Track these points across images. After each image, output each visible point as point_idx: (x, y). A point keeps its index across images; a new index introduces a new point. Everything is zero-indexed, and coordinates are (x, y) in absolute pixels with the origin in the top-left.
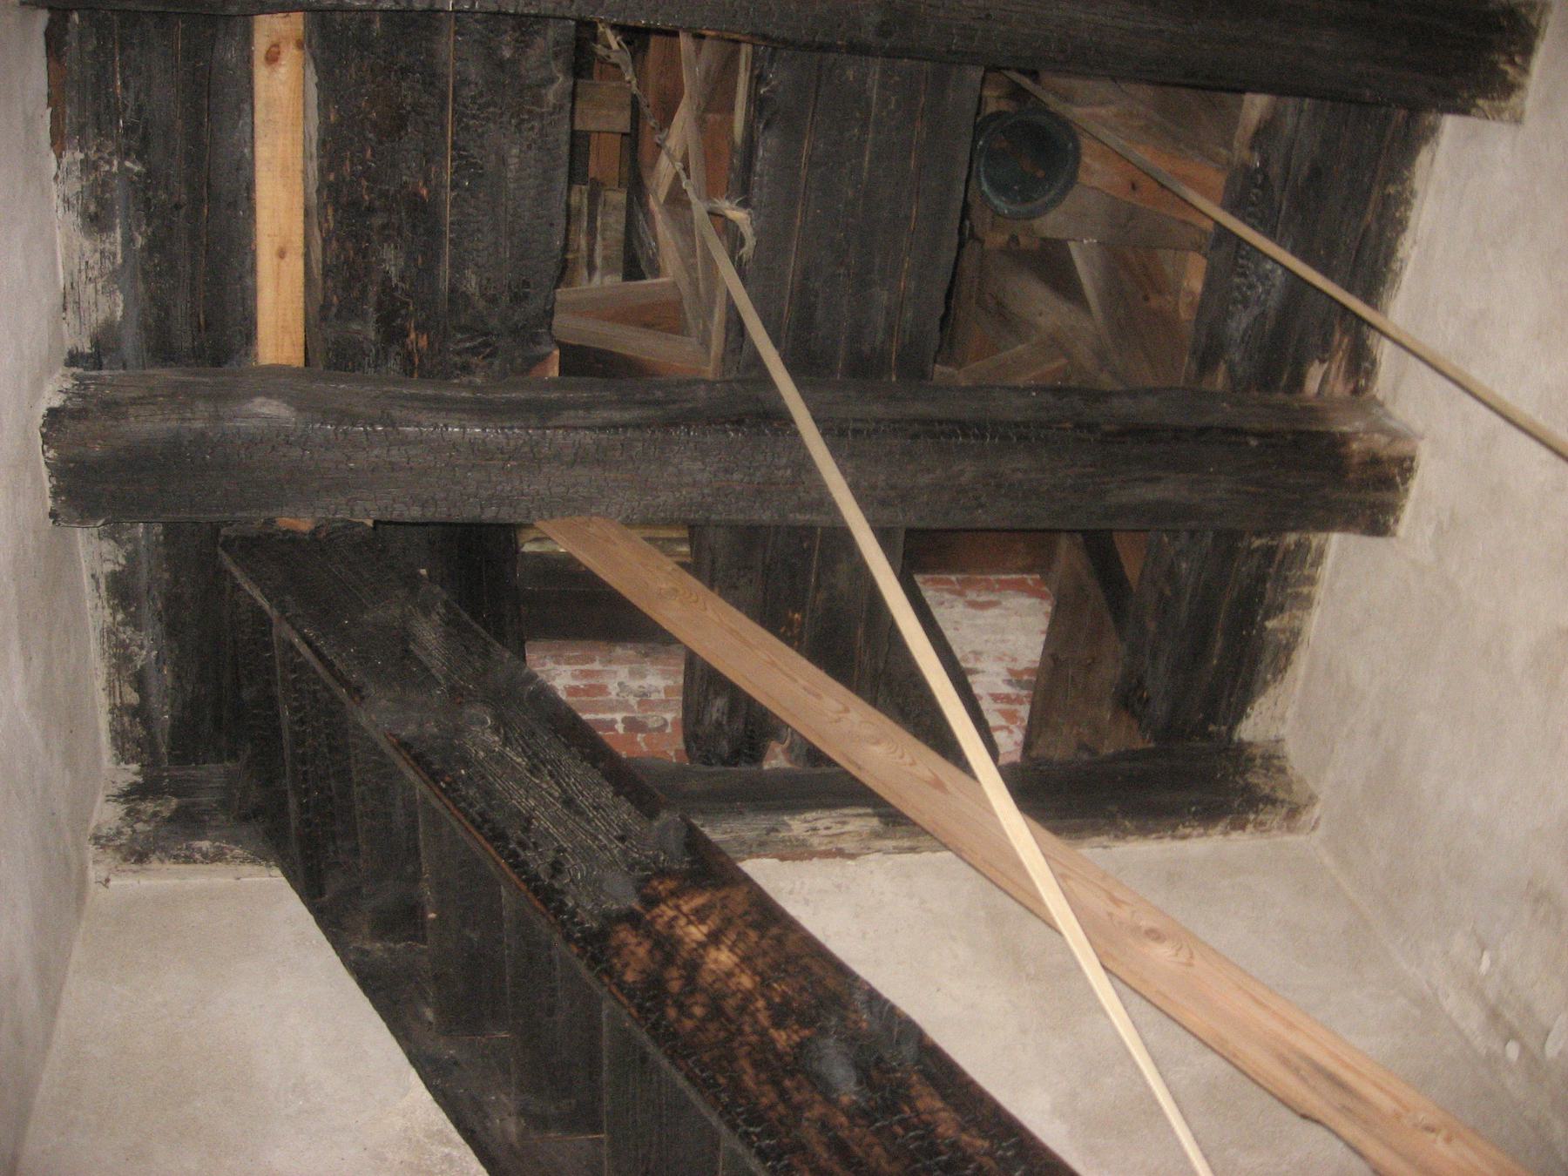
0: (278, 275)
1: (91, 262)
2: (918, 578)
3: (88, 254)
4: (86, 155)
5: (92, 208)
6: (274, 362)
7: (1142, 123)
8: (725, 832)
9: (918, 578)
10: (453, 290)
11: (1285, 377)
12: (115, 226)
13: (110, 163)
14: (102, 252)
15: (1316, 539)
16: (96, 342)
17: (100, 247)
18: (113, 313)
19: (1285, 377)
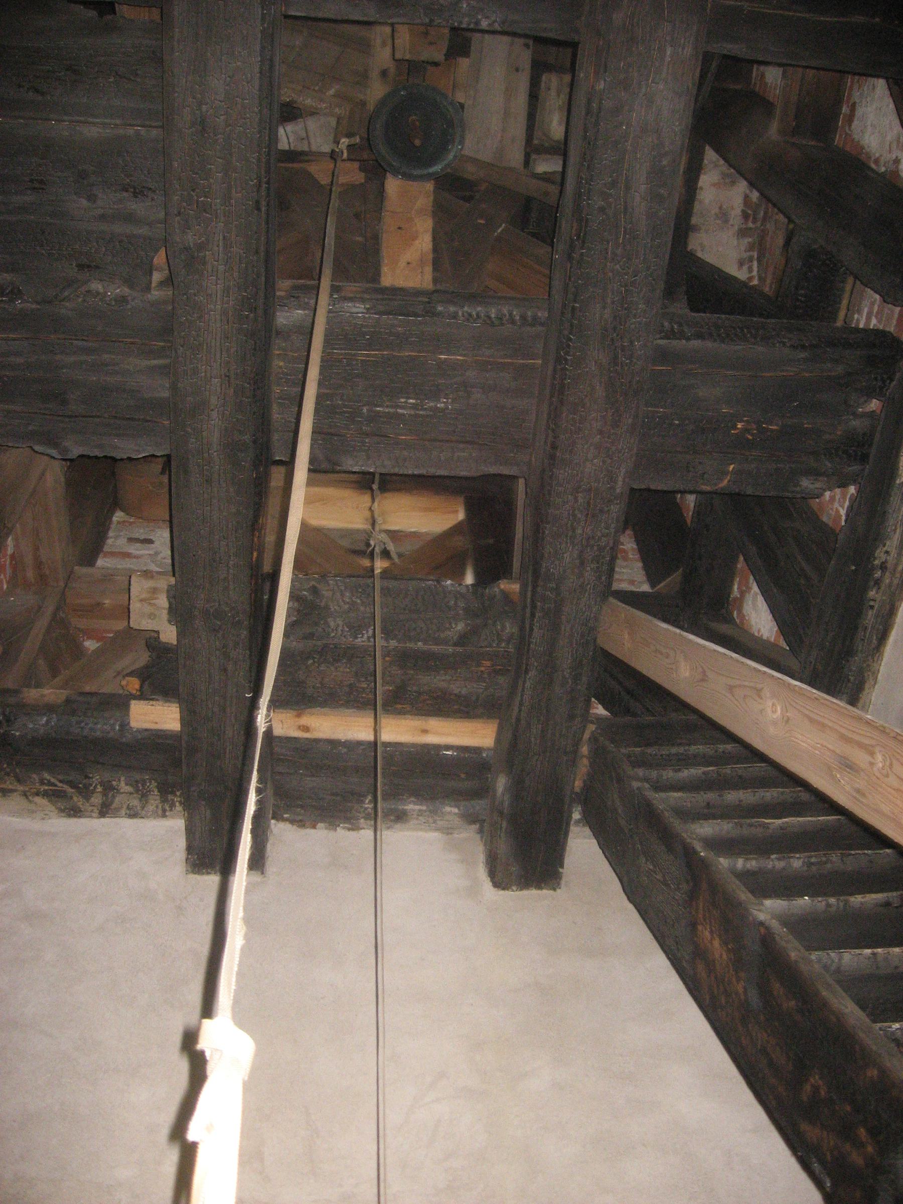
0: (436, 733)
1: (424, 821)
2: (710, 155)
3: (420, 822)
4: (362, 818)
5: (392, 818)
6: (494, 740)
7: (712, 166)
8: (895, 530)
9: (710, 155)
10: (455, 644)
11: (378, 409)
12: (403, 809)
13: (366, 809)
14: (418, 815)
15: (179, 808)
16: (474, 822)
17: (415, 816)
18: (455, 814)
19: (378, 409)
